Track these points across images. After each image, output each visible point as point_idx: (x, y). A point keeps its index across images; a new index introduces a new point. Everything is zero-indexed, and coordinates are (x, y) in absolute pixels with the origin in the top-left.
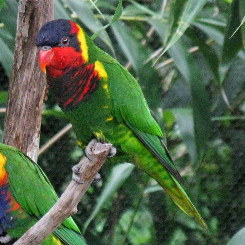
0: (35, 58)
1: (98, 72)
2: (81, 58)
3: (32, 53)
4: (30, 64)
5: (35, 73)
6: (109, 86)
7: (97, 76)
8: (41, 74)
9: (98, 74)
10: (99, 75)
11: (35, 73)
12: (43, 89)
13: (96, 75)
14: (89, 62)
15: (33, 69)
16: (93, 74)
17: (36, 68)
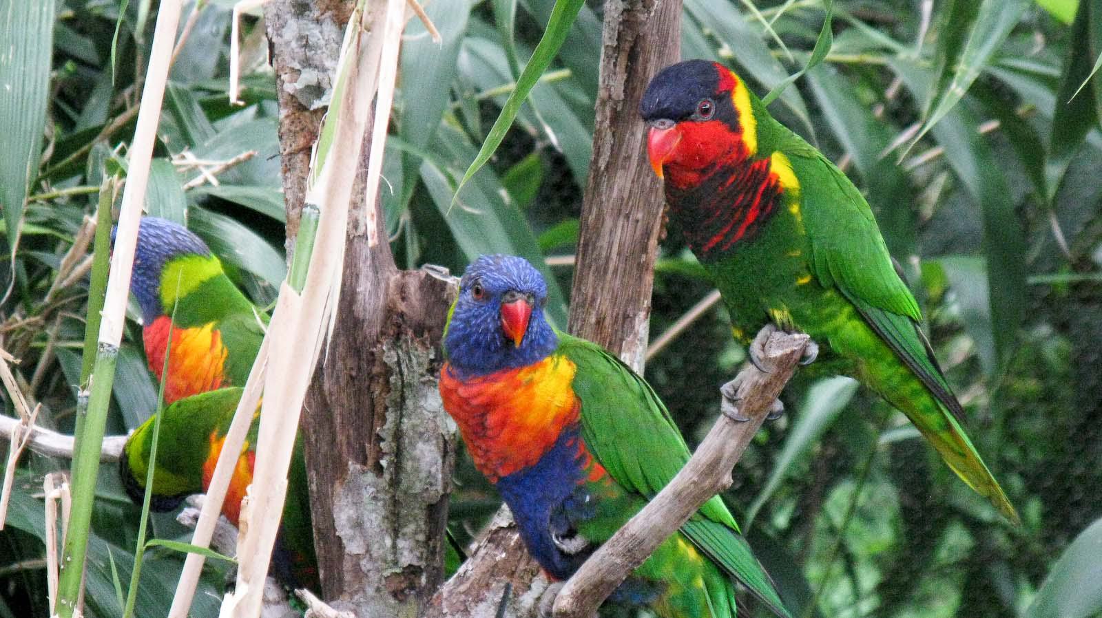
0: (638, 146)
1: (779, 178)
2: (741, 146)
3: (633, 134)
4: (628, 158)
5: (638, 178)
6: (801, 207)
7: (776, 186)
8: (652, 181)
9: (777, 181)
10: (780, 184)
11: (638, 178)
12: (657, 213)
13: (773, 183)
14: (758, 154)
15: (634, 171)
16: (767, 181)
17: (641, 168)
